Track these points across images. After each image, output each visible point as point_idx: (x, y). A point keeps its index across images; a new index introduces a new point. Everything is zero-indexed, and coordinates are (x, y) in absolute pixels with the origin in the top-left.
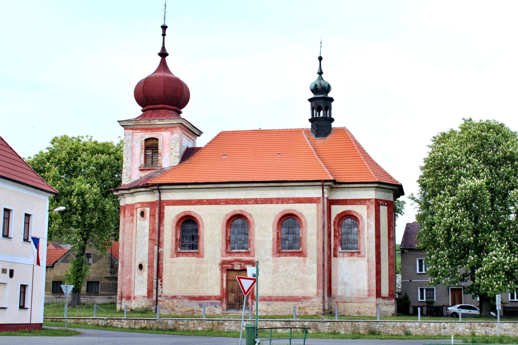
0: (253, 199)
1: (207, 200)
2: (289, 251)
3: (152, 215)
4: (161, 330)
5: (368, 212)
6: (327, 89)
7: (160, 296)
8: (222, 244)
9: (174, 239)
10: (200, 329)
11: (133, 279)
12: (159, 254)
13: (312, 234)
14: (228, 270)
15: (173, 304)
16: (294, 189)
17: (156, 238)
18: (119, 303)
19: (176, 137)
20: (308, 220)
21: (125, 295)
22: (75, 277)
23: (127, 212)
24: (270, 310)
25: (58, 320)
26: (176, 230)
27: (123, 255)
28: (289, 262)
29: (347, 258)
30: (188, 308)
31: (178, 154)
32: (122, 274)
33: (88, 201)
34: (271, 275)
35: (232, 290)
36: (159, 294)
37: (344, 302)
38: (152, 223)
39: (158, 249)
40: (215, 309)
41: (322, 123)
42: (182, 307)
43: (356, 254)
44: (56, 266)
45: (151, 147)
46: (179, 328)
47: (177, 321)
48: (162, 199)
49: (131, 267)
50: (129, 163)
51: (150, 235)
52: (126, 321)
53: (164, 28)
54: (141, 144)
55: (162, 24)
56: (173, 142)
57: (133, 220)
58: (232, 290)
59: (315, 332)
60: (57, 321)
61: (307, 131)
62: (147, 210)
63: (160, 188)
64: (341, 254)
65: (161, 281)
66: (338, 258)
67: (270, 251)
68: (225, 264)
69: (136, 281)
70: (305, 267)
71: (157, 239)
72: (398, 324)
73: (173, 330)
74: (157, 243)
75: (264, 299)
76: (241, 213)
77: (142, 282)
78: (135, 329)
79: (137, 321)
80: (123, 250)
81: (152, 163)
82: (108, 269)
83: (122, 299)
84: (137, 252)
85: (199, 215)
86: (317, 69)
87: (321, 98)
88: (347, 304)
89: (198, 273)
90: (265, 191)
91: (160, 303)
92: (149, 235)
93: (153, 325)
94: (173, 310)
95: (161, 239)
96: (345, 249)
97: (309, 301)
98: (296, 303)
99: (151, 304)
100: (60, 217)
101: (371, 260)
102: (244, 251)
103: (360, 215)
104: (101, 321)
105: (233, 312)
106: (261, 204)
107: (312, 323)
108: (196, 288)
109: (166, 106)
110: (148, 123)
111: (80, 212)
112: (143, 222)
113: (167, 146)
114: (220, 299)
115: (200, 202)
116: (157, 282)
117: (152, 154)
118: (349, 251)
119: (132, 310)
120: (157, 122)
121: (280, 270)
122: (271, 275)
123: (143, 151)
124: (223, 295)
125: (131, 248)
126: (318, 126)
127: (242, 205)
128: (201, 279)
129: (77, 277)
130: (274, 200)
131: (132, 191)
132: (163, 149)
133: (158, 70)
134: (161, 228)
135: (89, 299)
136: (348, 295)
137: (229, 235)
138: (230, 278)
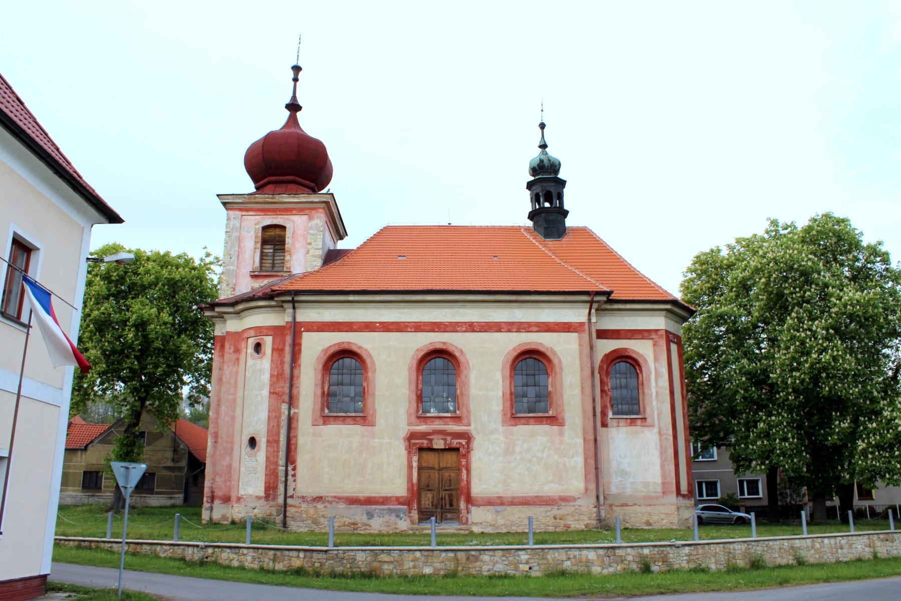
0: (465, 323)
2: (531, 415)
3: (278, 350)
4: (342, 576)
5: (655, 352)
6: (554, 167)
7: (292, 497)
8: (410, 402)
9: (319, 392)
10: (428, 570)
11: (235, 465)
12: (290, 420)
13: (572, 383)
14: (421, 449)
17: (285, 390)
18: (207, 509)
19: (317, 224)
20: (564, 361)
21: (219, 493)
23: (227, 345)
24: (501, 522)
25: (93, 544)
26: (323, 375)
27: (217, 423)
29: (624, 429)
30: (345, 519)
31: (320, 253)
32: (213, 455)
33: (152, 336)
34: (501, 458)
35: (428, 486)
37: (623, 505)
38: (278, 362)
39: (289, 410)
40: (398, 520)
43: (639, 422)
44: (90, 448)
45: (273, 240)
47: (376, 555)
48: (299, 319)
49: (232, 443)
50: (233, 265)
52: (251, 553)
53: (297, 69)
54: (256, 234)
55: (294, 63)
57: (238, 359)
58: (428, 486)
59: (664, 568)
60: (90, 548)
61: (527, 229)
62: (268, 342)
63: (296, 298)
64: (614, 422)
65: (294, 469)
66: (609, 429)
68: (415, 439)
69: (242, 469)
70: (561, 443)
71: (287, 390)
72: (786, 543)
73: (369, 576)
74: (286, 398)
78: (274, 572)
79: (278, 553)
80: (218, 413)
81: (273, 267)
82: (170, 455)
83: (212, 502)
84: (245, 415)
85: (366, 350)
87: (546, 182)
91: (291, 511)
92: (271, 386)
93: (322, 565)
94: (315, 522)
95: (295, 392)
96: (618, 414)
97: (572, 504)
98: (549, 508)
99: (274, 511)
100: (104, 361)
102: (449, 415)
103: (642, 356)
104: (190, 549)
105: (431, 527)
106: (480, 331)
107: (657, 549)
111: (137, 354)
112: (258, 362)
114: (407, 502)
115: (369, 327)
116: (287, 471)
117: (274, 252)
119: (233, 522)
121: (518, 449)
122: (501, 458)
123: (259, 245)
124: (413, 495)
125: (234, 411)
126: (547, 221)
127: (446, 334)
130: (503, 325)
131: (241, 307)
132: (293, 244)
134: (296, 372)
136: (629, 491)
137: (420, 386)
138: (424, 465)
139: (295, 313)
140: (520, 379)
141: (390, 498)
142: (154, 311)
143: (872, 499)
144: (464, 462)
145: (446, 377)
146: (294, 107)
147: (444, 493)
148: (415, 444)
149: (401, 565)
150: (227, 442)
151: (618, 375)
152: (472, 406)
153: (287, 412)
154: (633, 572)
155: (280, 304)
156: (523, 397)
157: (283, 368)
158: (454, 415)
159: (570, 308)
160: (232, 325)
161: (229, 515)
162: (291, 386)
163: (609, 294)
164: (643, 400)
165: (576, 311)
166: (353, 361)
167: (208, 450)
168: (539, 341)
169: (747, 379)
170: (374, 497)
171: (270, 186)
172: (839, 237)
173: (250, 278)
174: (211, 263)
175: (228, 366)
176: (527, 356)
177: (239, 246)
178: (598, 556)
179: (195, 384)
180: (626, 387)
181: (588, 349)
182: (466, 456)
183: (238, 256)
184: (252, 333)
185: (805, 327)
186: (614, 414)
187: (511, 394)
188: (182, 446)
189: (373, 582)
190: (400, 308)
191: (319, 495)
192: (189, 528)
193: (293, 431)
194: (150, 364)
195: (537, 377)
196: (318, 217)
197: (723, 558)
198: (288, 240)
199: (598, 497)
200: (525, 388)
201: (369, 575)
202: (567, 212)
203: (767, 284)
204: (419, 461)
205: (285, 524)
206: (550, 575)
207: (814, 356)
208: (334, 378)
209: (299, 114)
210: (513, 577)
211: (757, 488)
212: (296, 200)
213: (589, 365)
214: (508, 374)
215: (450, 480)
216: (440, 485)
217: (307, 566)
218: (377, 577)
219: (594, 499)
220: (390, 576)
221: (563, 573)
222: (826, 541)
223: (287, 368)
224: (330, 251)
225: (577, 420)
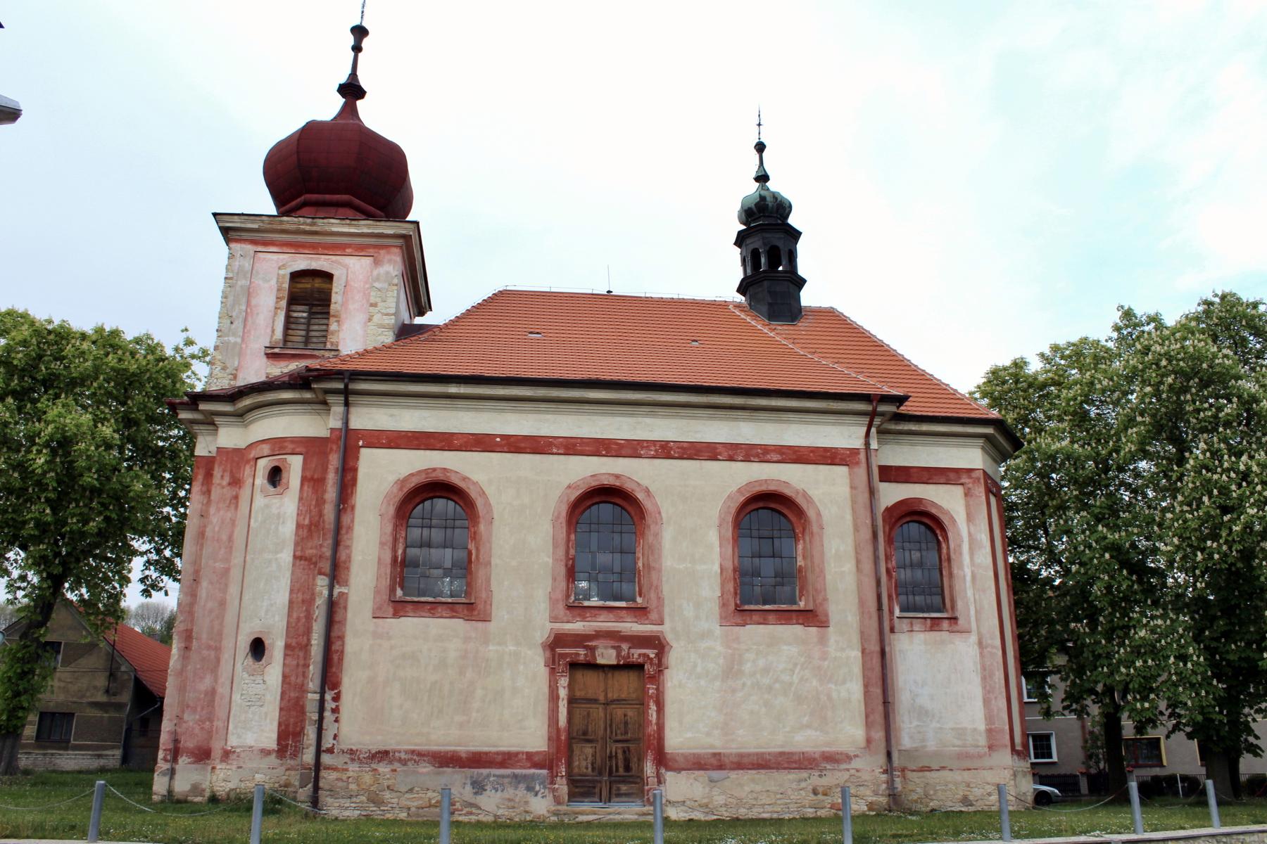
2: (767, 607)
3: (312, 481)
5: (968, 506)
7: (330, 751)
8: (554, 579)
9: (388, 557)
11: (222, 690)
13: (839, 551)
14: (574, 666)
15: (376, 781)
16: (781, 421)
17: (324, 550)
19: (388, 273)
21: (188, 743)
22: (9, 694)
23: (217, 472)
24: (719, 799)
26: (396, 527)
30: (430, 794)
32: (181, 673)
33: (82, 463)
34: (718, 684)
35: (585, 733)
36: (327, 742)
37: (922, 769)
42: (411, 790)
43: (945, 624)
45: (310, 297)
49: (218, 649)
50: (234, 335)
51: (300, 542)
53: (360, 32)
55: (358, 23)
56: (377, 285)
57: (236, 497)
58: (585, 733)
61: (738, 306)
62: (295, 465)
63: (353, 386)
64: (905, 625)
65: (337, 698)
67: (713, 607)
69: (236, 697)
70: (824, 657)
74: (326, 566)
82: (101, 681)
84: (246, 597)
87: (768, 233)
88: (933, 774)
89: (469, 674)
90: (692, 422)
91: (328, 777)
92: (296, 544)
94: (376, 800)
95: (342, 555)
98: (804, 774)
99: (295, 779)
102: (623, 604)
103: (947, 513)
109: (357, 202)
110: (308, 228)
111: (52, 495)
112: (275, 501)
113: (358, 297)
114: (545, 762)
115: (482, 443)
116: (322, 702)
117: (309, 319)
118: (926, 615)
119: (214, 799)
120: (336, 226)
121: (748, 667)
122: (718, 684)
123: (284, 303)
124: (558, 749)
125: (225, 589)
128: (479, 693)
129: (17, 694)
130: (720, 449)
132: (344, 304)
134: (346, 520)
135: (40, 758)
136: (932, 745)
137: (572, 552)
138: (578, 694)
139: (347, 413)
141: (517, 754)
142: (86, 418)
143: (1162, 766)
145: (617, 537)
146: (352, 90)
147: (614, 746)
148: (562, 656)
150: (209, 647)
151: (907, 545)
152: (666, 590)
153: (326, 592)
155: (321, 397)
156: (753, 575)
157: (321, 515)
158: (631, 604)
159: (834, 424)
160: (229, 437)
163: (901, 400)
164: (951, 587)
166: (451, 504)
167: (171, 663)
168: (784, 478)
169: (1112, 557)
170: (486, 753)
173: (264, 359)
174: (193, 357)
175: (218, 510)
176: (761, 504)
177: (248, 304)
179: (154, 557)
180: (921, 565)
181: (867, 495)
182: (657, 678)
183: (245, 320)
184: (266, 449)
185: (1226, 465)
186: (901, 611)
188: (123, 669)
190: (539, 412)
191: (382, 748)
192: (126, 809)
193: (336, 627)
194: (73, 515)
195: (777, 542)
196: (390, 261)
198: (334, 298)
199: (889, 755)
200: (756, 560)
202: (804, 281)
204: (571, 687)
205: (315, 802)
208: (415, 533)
209: (359, 103)
211: (1049, 747)
212: (346, 230)
213: (868, 521)
214: (729, 534)
215: (626, 723)
216: (608, 724)
219: (882, 759)
223: (329, 512)
225: (850, 618)
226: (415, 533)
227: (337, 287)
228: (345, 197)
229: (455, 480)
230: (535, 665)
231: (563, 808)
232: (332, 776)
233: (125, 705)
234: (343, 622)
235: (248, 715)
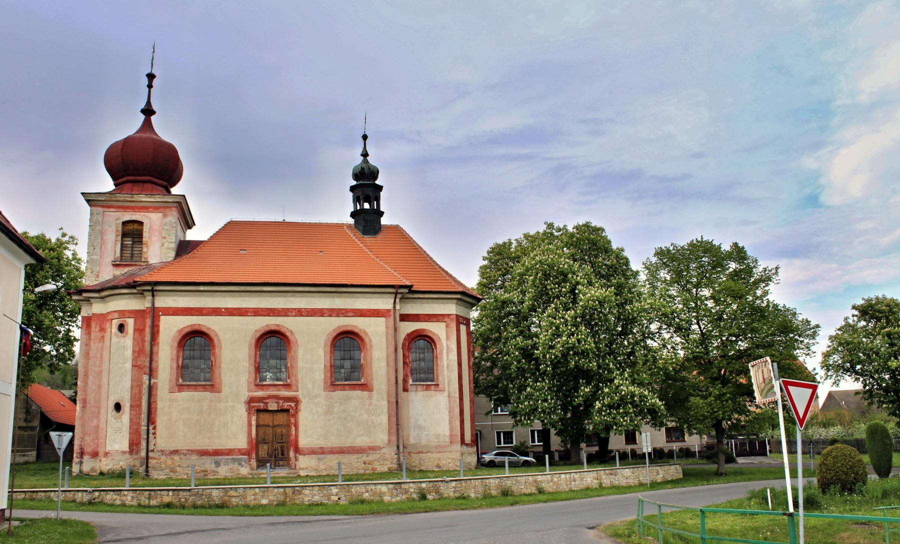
1: (226, 309)
3: (139, 330)
4: (203, 507)
5: (447, 332)
7: (153, 451)
9: (175, 365)
10: (264, 502)
11: (102, 425)
12: (150, 388)
13: (379, 357)
14: (259, 411)
21: (88, 449)
23: (93, 325)
26: (178, 352)
28: (347, 399)
29: (421, 393)
32: (82, 418)
36: (151, 447)
40: (240, 467)
41: (368, 220)
43: (433, 387)
45: (132, 233)
46: (230, 501)
47: (227, 492)
49: (99, 407)
51: (135, 359)
53: (151, 77)
55: (149, 71)
56: (166, 227)
57: (103, 337)
59: (437, 497)
61: (349, 226)
62: (130, 323)
64: (414, 388)
65: (154, 428)
69: (109, 429)
70: (370, 404)
71: (148, 364)
72: (530, 478)
74: (147, 370)
75: (313, 452)
76: (278, 329)
77: (120, 430)
78: (149, 506)
79: (153, 493)
84: (111, 384)
85: (213, 331)
86: (360, 150)
89: (213, 416)
90: (313, 299)
91: (152, 462)
92: (133, 360)
93: (186, 500)
94: (173, 471)
95: (154, 365)
96: (417, 381)
98: (360, 456)
99: (138, 464)
101: (452, 394)
103: (437, 335)
104: (80, 494)
105: (266, 472)
108: (210, 438)
112: (122, 340)
114: (247, 453)
115: (216, 312)
116: (148, 430)
117: (133, 244)
119: (102, 474)
120: (144, 198)
121: (336, 410)
123: (120, 238)
125: (100, 380)
126: (366, 221)
128: (217, 424)
132: (150, 238)
133: (139, 131)
134: (155, 349)
136: (424, 442)
138: (261, 423)
140: (338, 354)
143: (684, 441)
144: (293, 420)
146: (148, 112)
148: (253, 407)
149: (246, 498)
152: (300, 377)
154: (413, 500)
157: (143, 346)
160: (98, 308)
161: (97, 468)
162: (151, 360)
165: (384, 300)
168: (354, 324)
171: (128, 185)
172: (594, 243)
178: (389, 489)
180: (424, 360)
182: (295, 415)
184: (116, 315)
187: (331, 366)
189: (225, 511)
197: (480, 489)
198: (145, 234)
199: (398, 447)
201: (222, 506)
203: (534, 281)
204: (257, 420)
205: (147, 471)
206: (353, 503)
207: (564, 338)
209: (153, 118)
210: (326, 505)
211: (512, 438)
212: (149, 200)
214: (329, 350)
216: (274, 440)
217: (175, 501)
218: (228, 507)
219: (395, 448)
220: (237, 506)
221: (363, 502)
222: (563, 476)
224: (180, 241)
226: (187, 353)
227: (146, 229)
228: (147, 178)
229: (204, 329)
230: (242, 410)
231: (255, 472)
232: (154, 461)
233: (35, 427)
234: (156, 395)
235: (115, 438)
